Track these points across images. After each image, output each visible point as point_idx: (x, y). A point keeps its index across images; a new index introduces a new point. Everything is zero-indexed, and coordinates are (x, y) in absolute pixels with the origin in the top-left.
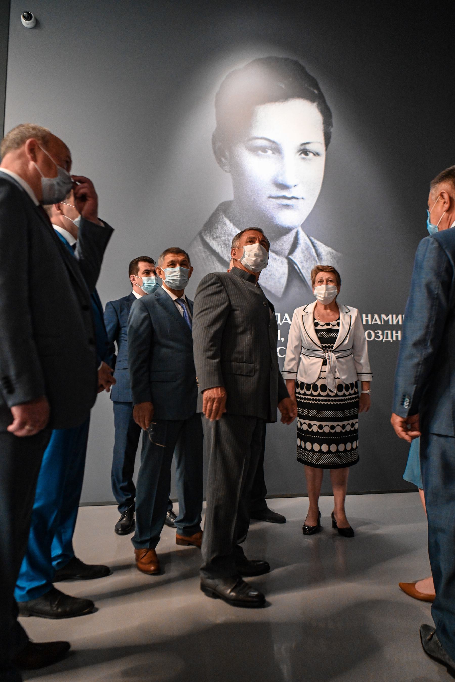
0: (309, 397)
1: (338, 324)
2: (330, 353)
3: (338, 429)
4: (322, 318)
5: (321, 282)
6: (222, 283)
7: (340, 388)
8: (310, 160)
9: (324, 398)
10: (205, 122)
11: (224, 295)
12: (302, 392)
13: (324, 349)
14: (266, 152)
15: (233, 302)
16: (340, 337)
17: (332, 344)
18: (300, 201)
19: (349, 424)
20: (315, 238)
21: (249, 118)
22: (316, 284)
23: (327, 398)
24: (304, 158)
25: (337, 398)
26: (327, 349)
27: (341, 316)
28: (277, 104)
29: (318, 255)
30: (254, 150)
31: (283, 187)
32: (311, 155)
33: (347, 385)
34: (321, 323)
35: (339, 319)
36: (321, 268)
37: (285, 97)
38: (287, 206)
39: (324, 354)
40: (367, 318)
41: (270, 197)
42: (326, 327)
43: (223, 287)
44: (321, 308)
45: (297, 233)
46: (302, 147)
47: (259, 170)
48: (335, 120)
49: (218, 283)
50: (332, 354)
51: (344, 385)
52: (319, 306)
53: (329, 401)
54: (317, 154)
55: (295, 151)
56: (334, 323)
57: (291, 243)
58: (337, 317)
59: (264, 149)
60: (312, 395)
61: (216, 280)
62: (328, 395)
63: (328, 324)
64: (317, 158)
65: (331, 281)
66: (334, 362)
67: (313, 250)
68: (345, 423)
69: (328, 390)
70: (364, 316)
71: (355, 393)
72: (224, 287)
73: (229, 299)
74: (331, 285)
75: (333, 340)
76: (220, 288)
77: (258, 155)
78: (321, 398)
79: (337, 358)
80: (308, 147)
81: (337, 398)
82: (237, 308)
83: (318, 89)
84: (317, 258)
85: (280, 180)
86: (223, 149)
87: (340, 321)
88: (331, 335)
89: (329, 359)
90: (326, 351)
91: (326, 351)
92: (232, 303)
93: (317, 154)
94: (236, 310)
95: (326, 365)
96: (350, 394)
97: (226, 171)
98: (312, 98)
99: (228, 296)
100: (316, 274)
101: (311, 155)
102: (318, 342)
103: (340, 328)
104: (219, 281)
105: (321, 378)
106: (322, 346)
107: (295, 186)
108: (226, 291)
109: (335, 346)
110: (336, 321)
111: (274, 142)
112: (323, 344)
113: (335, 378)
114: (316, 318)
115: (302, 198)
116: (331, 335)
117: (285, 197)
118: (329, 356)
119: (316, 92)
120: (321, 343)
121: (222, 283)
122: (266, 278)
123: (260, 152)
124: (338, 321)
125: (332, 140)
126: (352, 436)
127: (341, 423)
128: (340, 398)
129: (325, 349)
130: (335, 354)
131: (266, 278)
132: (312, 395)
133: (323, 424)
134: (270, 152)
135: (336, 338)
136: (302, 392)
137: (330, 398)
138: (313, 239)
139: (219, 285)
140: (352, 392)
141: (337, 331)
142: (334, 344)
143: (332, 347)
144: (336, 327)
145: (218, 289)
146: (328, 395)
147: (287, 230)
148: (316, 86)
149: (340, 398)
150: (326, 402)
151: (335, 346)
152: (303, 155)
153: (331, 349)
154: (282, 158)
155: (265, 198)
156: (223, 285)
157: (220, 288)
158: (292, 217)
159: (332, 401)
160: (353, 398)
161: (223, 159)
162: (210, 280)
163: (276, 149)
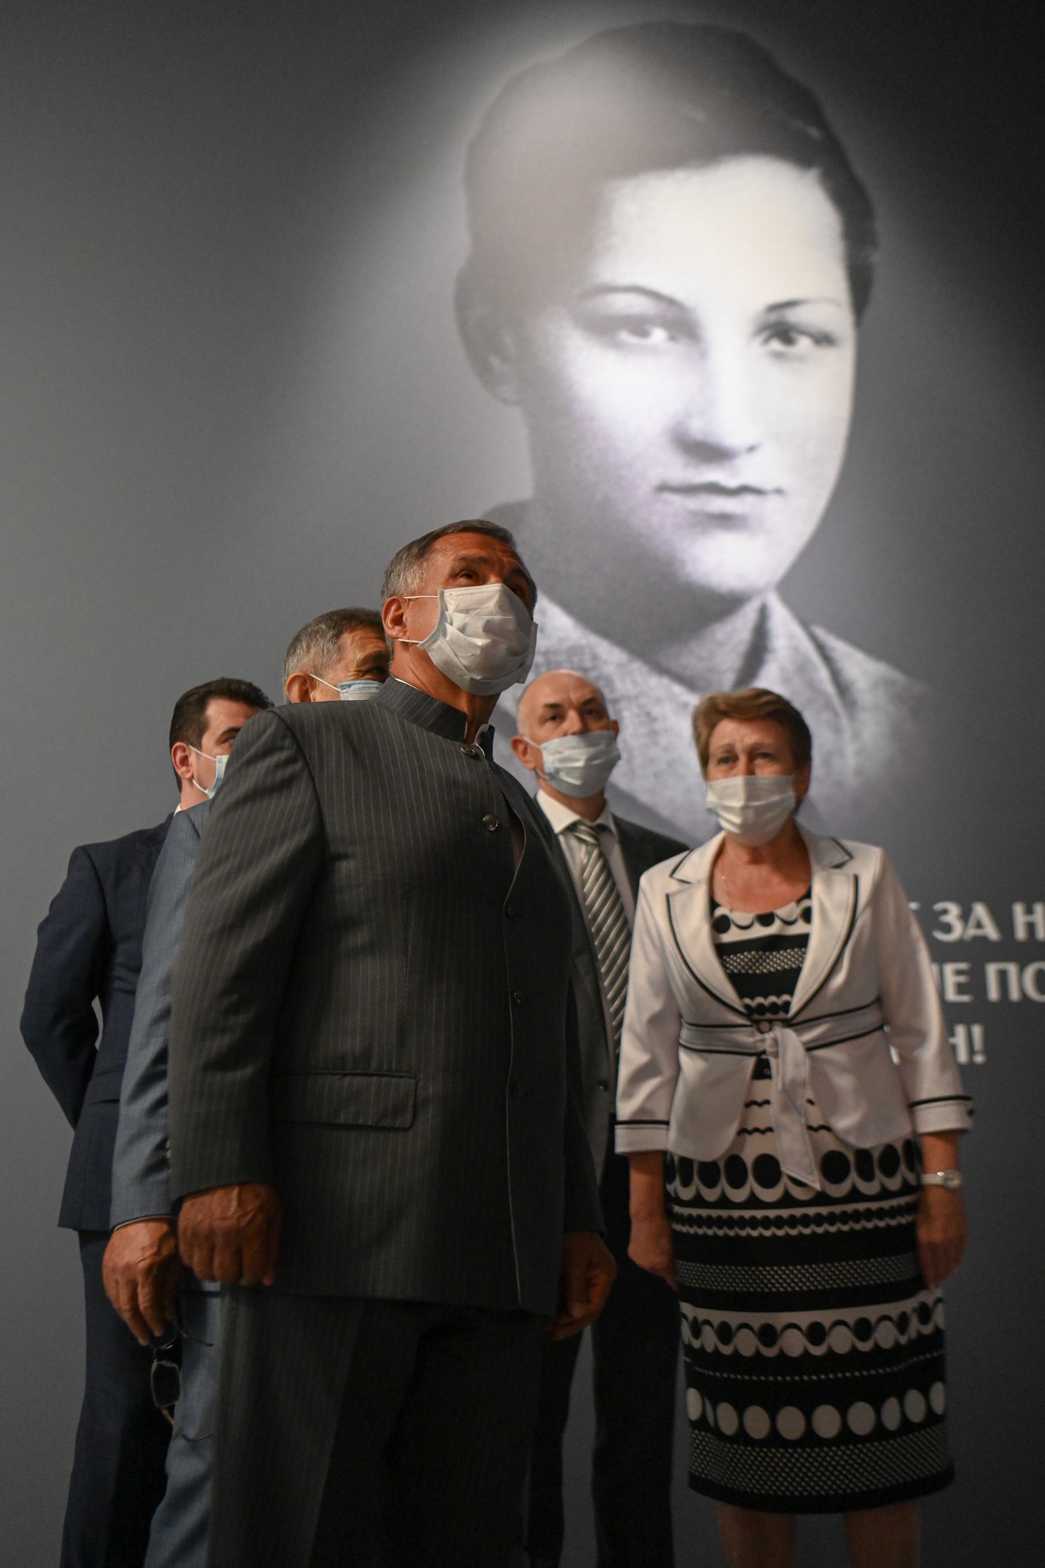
0: (850, 1208)
1: (807, 915)
2: (779, 1032)
3: (841, 1341)
4: (746, 896)
5: (729, 758)
6: (300, 749)
7: (833, 1165)
8: (801, 359)
9: (772, 1214)
10: (432, 239)
11: (299, 796)
12: (738, 1195)
13: (756, 1017)
14: (644, 333)
15: (336, 825)
16: (815, 964)
17: (786, 997)
18: (771, 503)
19: (885, 1318)
20: (831, 629)
21: (584, 223)
22: (712, 766)
23: (785, 1213)
24: (778, 356)
25: (824, 1210)
26: (769, 1016)
27: (818, 888)
28: (680, 175)
29: (843, 688)
30: (606, 329)
31: (708, 452)
32: (804, 344)
33: (863, 1155)
34: (741, 917)
35: (808, 895)
36: (722, 707)
37: (707, 152)
38: (726, 521)
39: (759, 1037)
40: (1030, 918)
41: (664, 488)
42: (759, 931)
43: (298, 766)
44: (736, 855)
45: (763, 614)
46: (773, 317)
47: (623, 396)
48: (883, 225)
49: (282, 749)
50: (790, 1033)
51: (851, 1158)
52: (731, 852)
53: (792, 1222)
54: (823, 339)
55: (746, 327)
56: (790, 910)
57: (743, 648)
58: (801, 890)
59: (639, 326)
60: (753, 1202)
61: (274, 736)
62: (787, 1200)
63: (766, 919)
64: (828, 354)
65: (765, 755)
66: (797, 1065)
67: (823, 674)
68: (871, 1312)
69: (785, 1180)
70: (1018, 909)
71: (907, 1188)
72: (306, 764)
73: (320, 813)
74: (767, 772)
75: (788, 980)
76: (289, 771)
77: (618, 346)
78: (759, 1214)
79: (810, 1048)
80: (793, 316)
81: (824, 1210)
82: (350, 850)
83: (823, 125)
84: (836, 701)
85: (697, 428)
86: (498, 329)
87: (814, 903)
88: (778, 961)
89: (776, 1055)
90: (765, 1026)
91: (765, 1026)
92: (328, 829)
93: (823, 339)
94: (346, 857)
95: (769, 1077)
96: (885, 1194)
97: (505, 401)
98: (799, 152)
99: (317, 798)
100: (712, 726)
101: (804, 344)
102: (727, 991)
103: (815, 930)
104: (287, 742)
105: (757, 1130)
106: (747, 1007)
107: (751, 449)
108: (312, 778)
109: (797, 1001)
110: (799, 901)
111: (670, 302)
112: (747, 1001)
113: (810, 1128)
114: (719, 898)
115: (779, 491)
116: (778, 961)
117: (715, 489)
118: (775, 1041)
119: (814, 132)
120: (741, 995)
121: (300, 749)
122: (656, 775)
123: (625, 336)
124: (805, 903)
125: (879, 292)
126: (920, 1363)
127: (851, 1315)
128: (837, 1209)
129: (757, 1018)
130: (799, 1032)
131: (656, 775)
132: (753, 1202)
133: (825, 1317)
134: (659, 335)
135: (796, 972)
136: (738, 1195)
137: (798, 1212)
138: (820, 632)
139: (284, 755)
140: (894, 1184)
141: (802, 941)
142: (791, 992)
143: (787, 1005)
144: (799, 928)
145: (280, 775)
146: (787, 1200)
147: (724, 604)
148: (813, 113)
149: (837, 1209)
150: (780, 1228)
151: (797, 1001)
152: (776, 345)
153: (781, 1015)
154: (703, 355)
155: (644, 490)
156: (300, 753)
157: (289, 771)
158: (744, 558)
159: (806, 1220)
160: (893, 1213)
161: (495, 362)
162: (259, 737)
163: (682, 324)
